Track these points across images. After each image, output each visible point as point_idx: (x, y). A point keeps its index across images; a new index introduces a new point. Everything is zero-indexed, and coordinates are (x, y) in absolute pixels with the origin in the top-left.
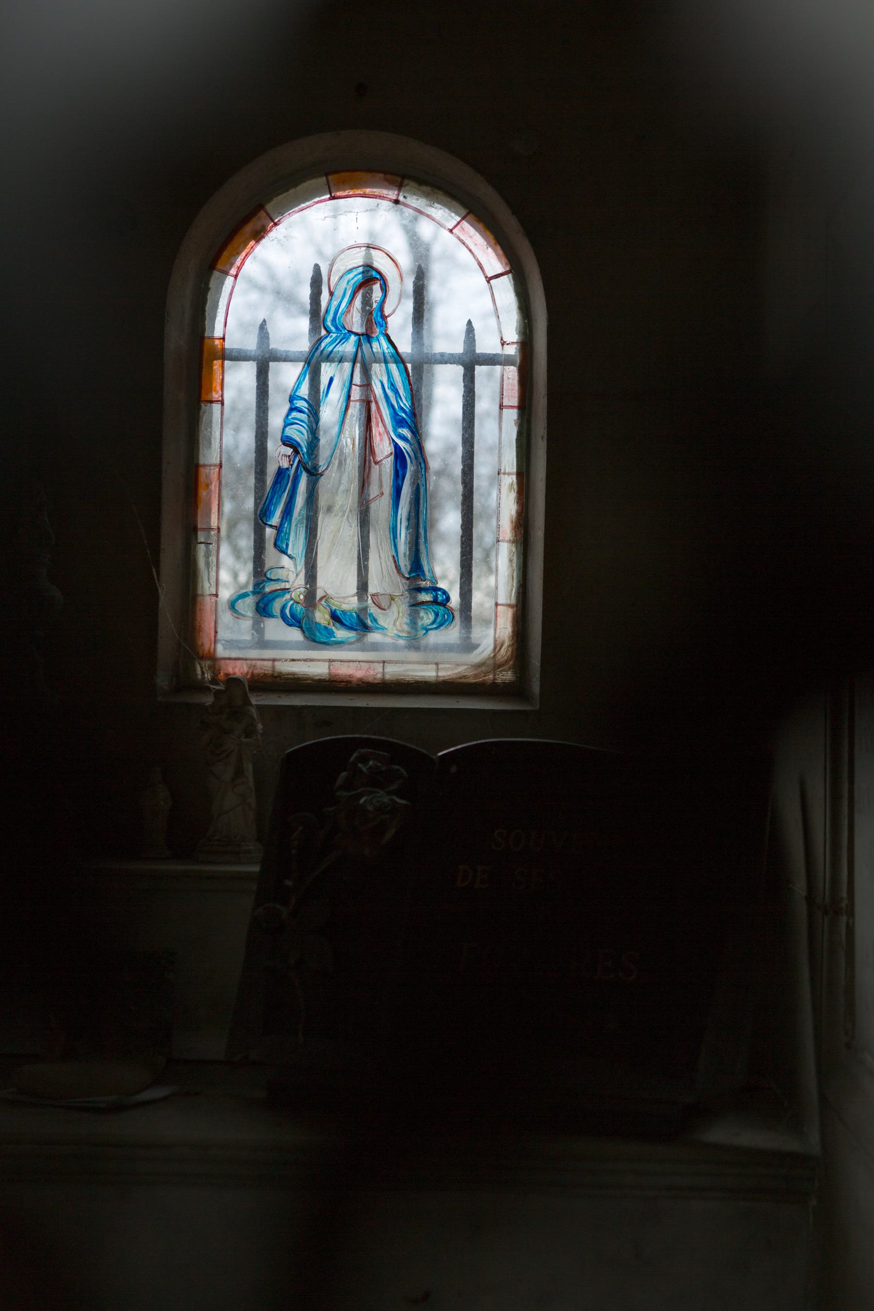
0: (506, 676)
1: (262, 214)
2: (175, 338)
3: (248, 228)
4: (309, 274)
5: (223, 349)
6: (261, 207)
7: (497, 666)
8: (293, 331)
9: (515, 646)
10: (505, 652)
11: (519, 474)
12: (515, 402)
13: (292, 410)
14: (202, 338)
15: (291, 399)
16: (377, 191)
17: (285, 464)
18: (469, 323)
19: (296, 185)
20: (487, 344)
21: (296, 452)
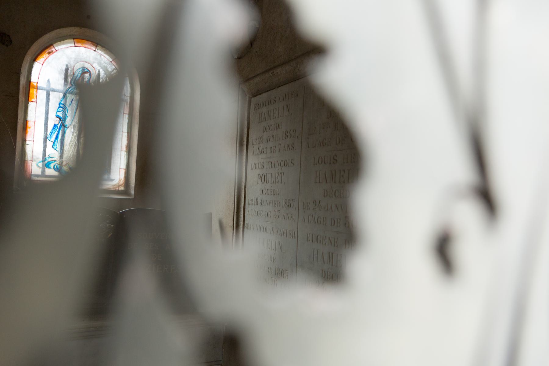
0: (122, 188)
1: (52, 47)
2: (23, 81)
3: (48, 50)
4: (64, 68)
5: (37, 86)
6: (52, 45)
7: (120, 186)
8: (58, 83)
9: (106, 177)
10: (122, 182)
11: (128, 133)
12: (128, 113)
13: (59, 107)
14: (30, 82)
15: (59, 104)
16: (87, 46)
17: (57, 123)
18: (49, 80)
19: (64, 40)
20: (53, 86)
21: (60, 120)
